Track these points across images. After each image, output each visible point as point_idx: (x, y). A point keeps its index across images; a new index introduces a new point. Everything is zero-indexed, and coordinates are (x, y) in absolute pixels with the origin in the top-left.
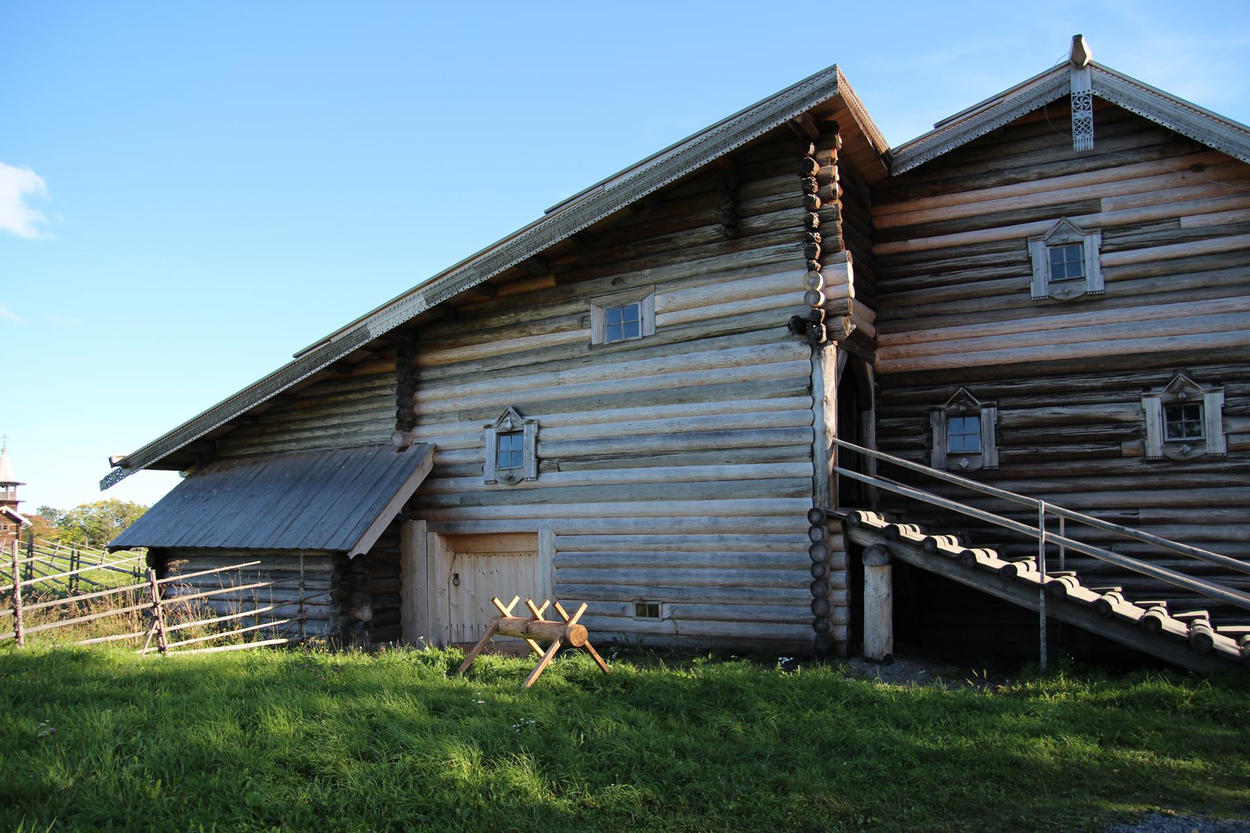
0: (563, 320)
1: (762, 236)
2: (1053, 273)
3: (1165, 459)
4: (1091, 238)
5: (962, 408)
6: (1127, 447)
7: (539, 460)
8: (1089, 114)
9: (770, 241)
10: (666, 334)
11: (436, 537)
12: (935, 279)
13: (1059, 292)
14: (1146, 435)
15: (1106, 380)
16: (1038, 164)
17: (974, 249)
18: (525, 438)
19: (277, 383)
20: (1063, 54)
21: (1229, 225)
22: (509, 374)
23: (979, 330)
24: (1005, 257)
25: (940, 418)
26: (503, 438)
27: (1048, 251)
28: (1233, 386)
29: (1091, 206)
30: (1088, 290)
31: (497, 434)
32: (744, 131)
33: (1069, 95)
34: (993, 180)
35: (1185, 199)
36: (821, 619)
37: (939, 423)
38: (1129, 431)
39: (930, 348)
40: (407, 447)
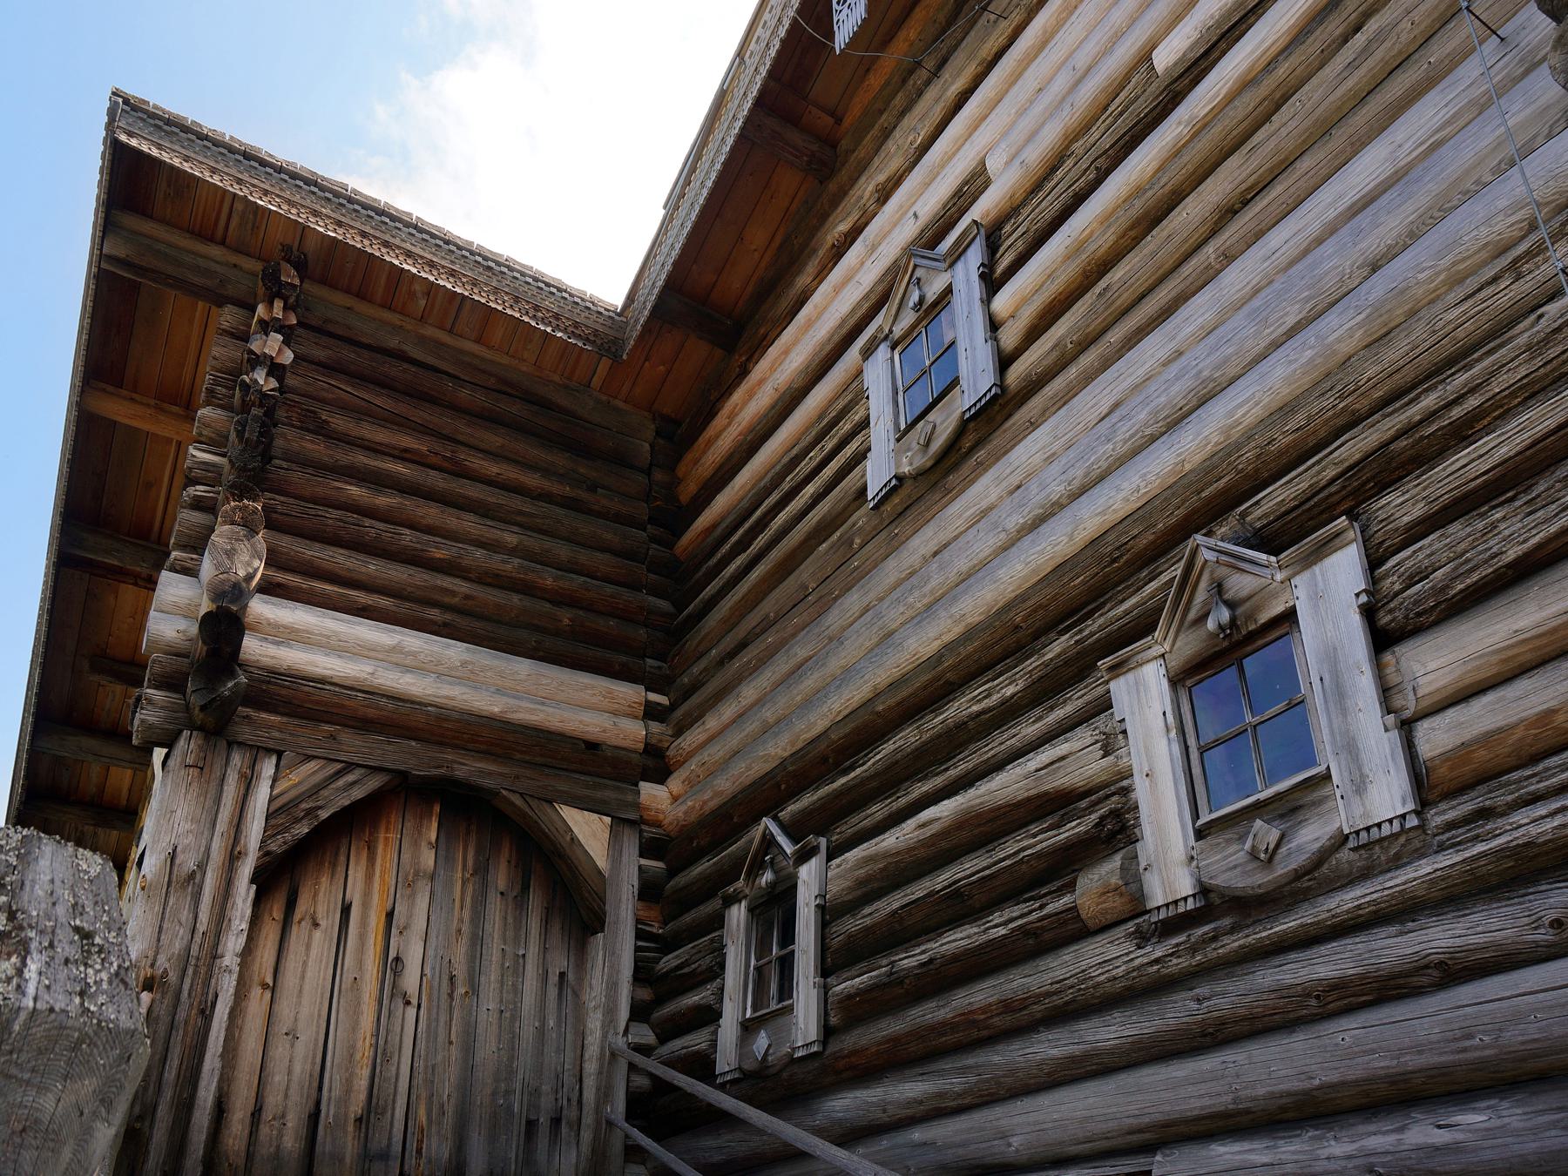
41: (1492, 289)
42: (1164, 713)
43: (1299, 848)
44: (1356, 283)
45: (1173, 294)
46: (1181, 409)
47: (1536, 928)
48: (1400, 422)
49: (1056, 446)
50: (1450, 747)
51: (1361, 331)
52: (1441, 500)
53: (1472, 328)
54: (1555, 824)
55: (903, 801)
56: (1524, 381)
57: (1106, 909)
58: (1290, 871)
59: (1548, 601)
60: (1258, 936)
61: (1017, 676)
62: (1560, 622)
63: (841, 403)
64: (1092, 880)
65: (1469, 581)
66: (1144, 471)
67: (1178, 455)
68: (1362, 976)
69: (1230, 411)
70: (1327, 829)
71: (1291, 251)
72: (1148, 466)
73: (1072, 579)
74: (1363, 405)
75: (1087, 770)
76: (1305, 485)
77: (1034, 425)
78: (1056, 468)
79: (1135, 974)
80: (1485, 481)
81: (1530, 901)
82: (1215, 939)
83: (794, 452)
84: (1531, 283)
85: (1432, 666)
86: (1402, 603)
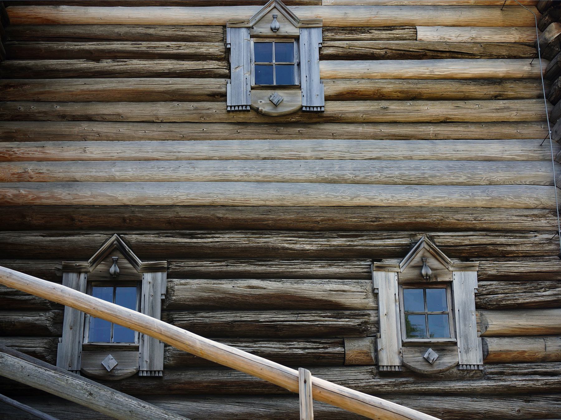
4: (310, 34)
14: (378, 330)
23: (149, 149)
27: (252, 43)
30: (305, 104)
39: (78, 172)
41: (526, 219)
42: (395, 294)
43: (443, 363)
44: (484, 184)
45: (413, 133)
46: (411, 181)
47: (513, 410)
48: (493, 241)
49: (347, 155)
50: (497, 350)
51: (485, 202)
52: (502, 273)
53: (516, 226)
54: (523, 383)
55: (231, 269)
56: (527, 252)
57: (358, 359)
58: (439, 370)
59: (529, 320)
60: (422, 388)
61: (314, 243)
62: (530, 327)
63: (195, 32)
64: (354, 346)
65: (507, 303)
66: (394, 195)
67: (409, 198)
68: (459, 411)
69: (434, 197)
70: (454, 360)
71: (463, 155)
72: (396, 194)
73: (351, 218)
74: (479, 226)
75: (354, 300)
76: (458, 241)
77: (334, 136)
78: (355, 164)
79: (368, 387)
80: (514, 275)
81: (512, 403)
82: (405, 384)
83: (151, 31)
84: (535, 224)
85: (494, 323)
86: (485, 298)
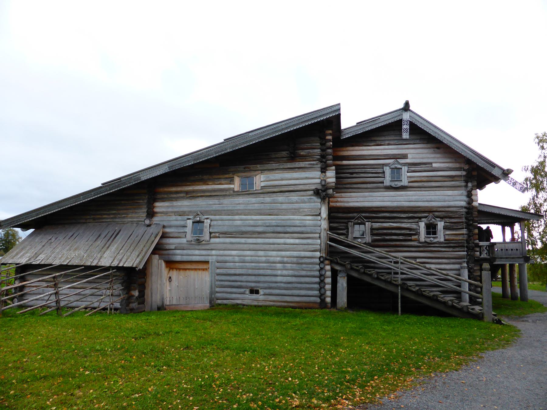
0: (222, 180)
1: (304, 158)
2: (391, 178)
3: (426, 242)
5: (359, 221)
6: (413, 237)
7: (210, 233)
8: (408, 127)
9: (307, 160)
10: (265, 189)
11: (163, 262)
12: (352, 176)
13: (393, 184)
15: (407, 215)
16: (388, 140)
17: (365, 167)
18: (205, 224)
19: (91, 195)
20: (402, 106)
21: (447, 167)
22: (198, 199)
24: (375, 170)
25: (351, 225)
26: (194, 224)
28: (447, 220)
29: (405, 156)
31: (193, 222)
32: (305, 121)
33: (402, 119)
34: (373, 144)
35: (434, 158)
36: (322, 296)
37: (351, 226)
38: (414, 232)
40: (151, 225)
